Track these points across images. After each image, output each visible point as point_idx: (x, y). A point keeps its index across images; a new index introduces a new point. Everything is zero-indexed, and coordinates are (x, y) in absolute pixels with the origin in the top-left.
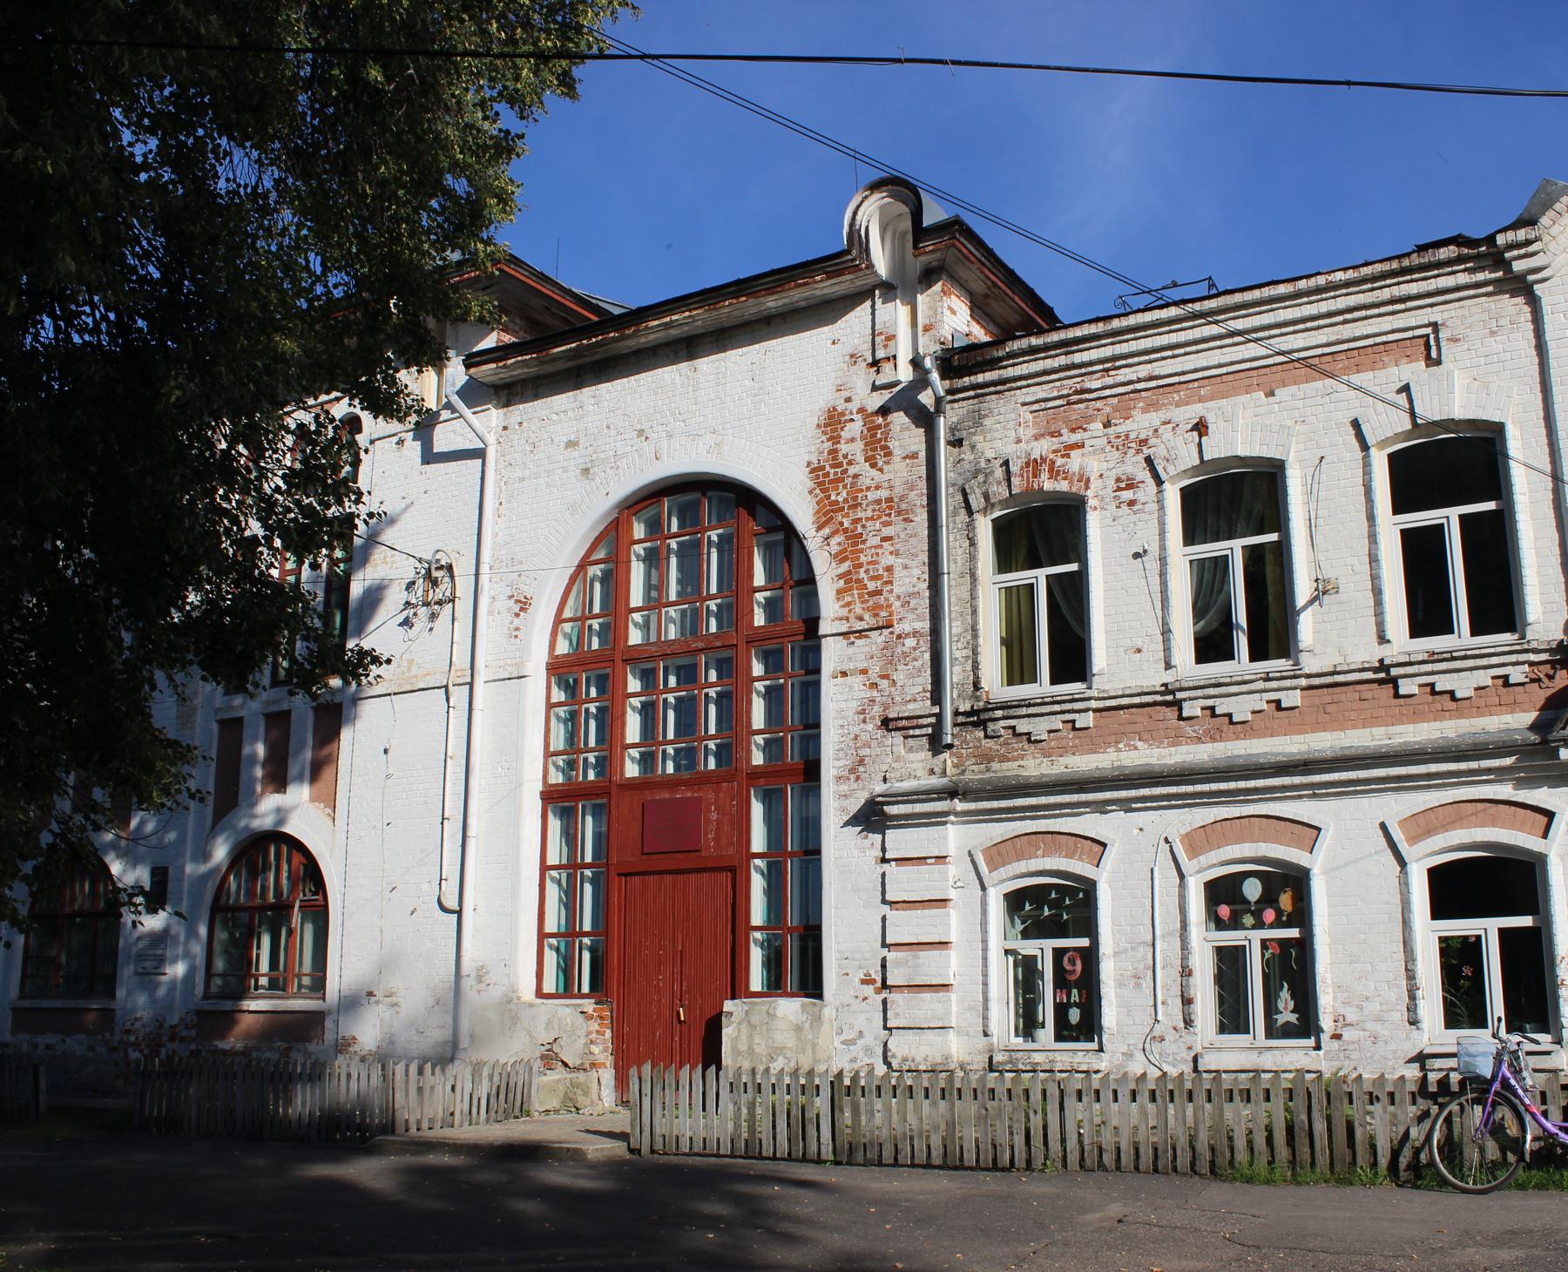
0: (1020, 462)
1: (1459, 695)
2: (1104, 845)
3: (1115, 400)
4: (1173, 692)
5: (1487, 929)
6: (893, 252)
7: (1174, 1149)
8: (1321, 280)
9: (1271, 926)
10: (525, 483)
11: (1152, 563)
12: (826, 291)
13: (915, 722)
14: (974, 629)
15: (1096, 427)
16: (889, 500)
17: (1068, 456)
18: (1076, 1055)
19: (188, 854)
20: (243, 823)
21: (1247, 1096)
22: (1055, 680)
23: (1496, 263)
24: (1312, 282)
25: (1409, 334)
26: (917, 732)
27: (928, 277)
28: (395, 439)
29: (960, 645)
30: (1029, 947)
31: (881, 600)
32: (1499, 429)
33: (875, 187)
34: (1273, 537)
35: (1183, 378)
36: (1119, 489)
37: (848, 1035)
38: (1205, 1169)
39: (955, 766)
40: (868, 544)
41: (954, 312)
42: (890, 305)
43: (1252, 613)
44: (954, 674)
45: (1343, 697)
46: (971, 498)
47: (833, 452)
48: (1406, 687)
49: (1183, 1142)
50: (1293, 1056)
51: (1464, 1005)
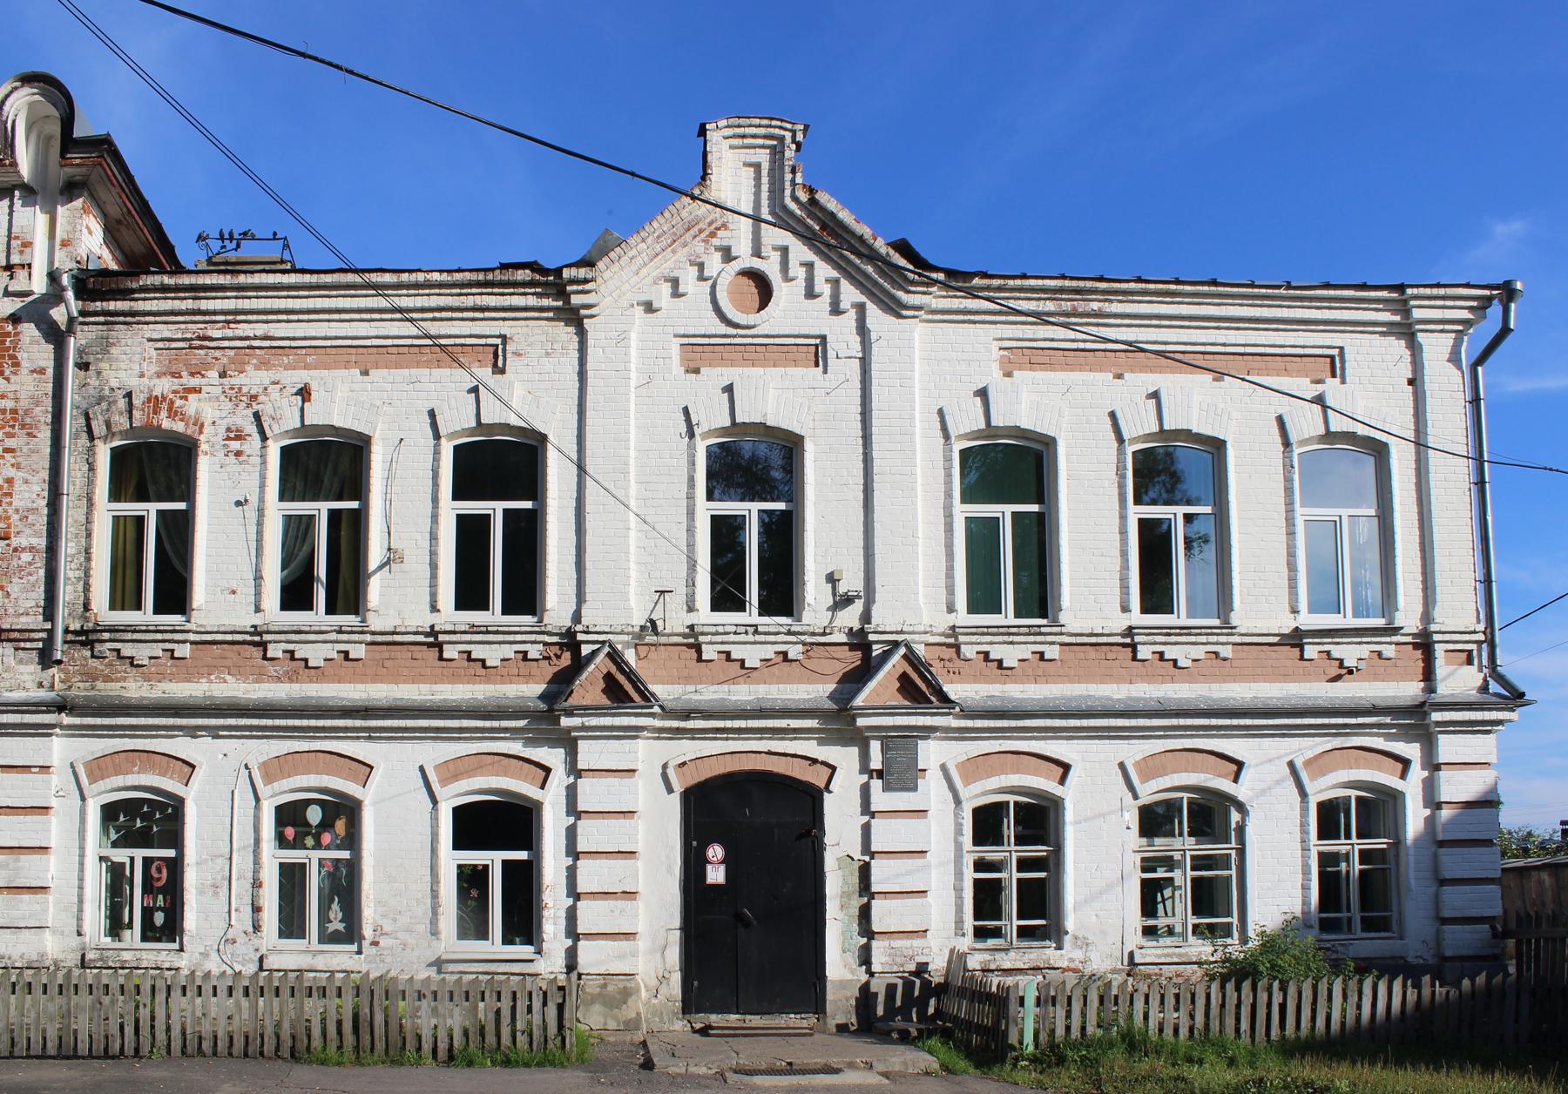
0: (143, 397)
1: (488, 663)
2: (193, 767)
3: (232, 353)
4: (260, 634)
5: (493, 859)
6: (37, 154)
7: (262, 1036)
8: (421, 277)
9: (328, 848)
13: (26, 635)
14: (88, 551)
15: (213, 375)
17: (186, 399)
18: (159, 954)
21: (323, 992)
22: (157, 611)
23: (557, 290)
24: (413, 277)
25: (482, 341)
26: (28, 645)
27: (70, 190)
29: (73, 566)
30: (121, 855)
32: (1050, 443)
33: (28, 79)
34: (354, 505)
35: (294, 344)
36: (228, 438)
38: (287, 1054)
39: (62, 681)
41: (90, 233)
42: (29, 210)
43: (327, 570)
44: (67, 593)
45: (398, 655)
46: (94, 424)
48: (449, 652)
49: (269, 1031)
50: (340, 958)
51: (473, 923)
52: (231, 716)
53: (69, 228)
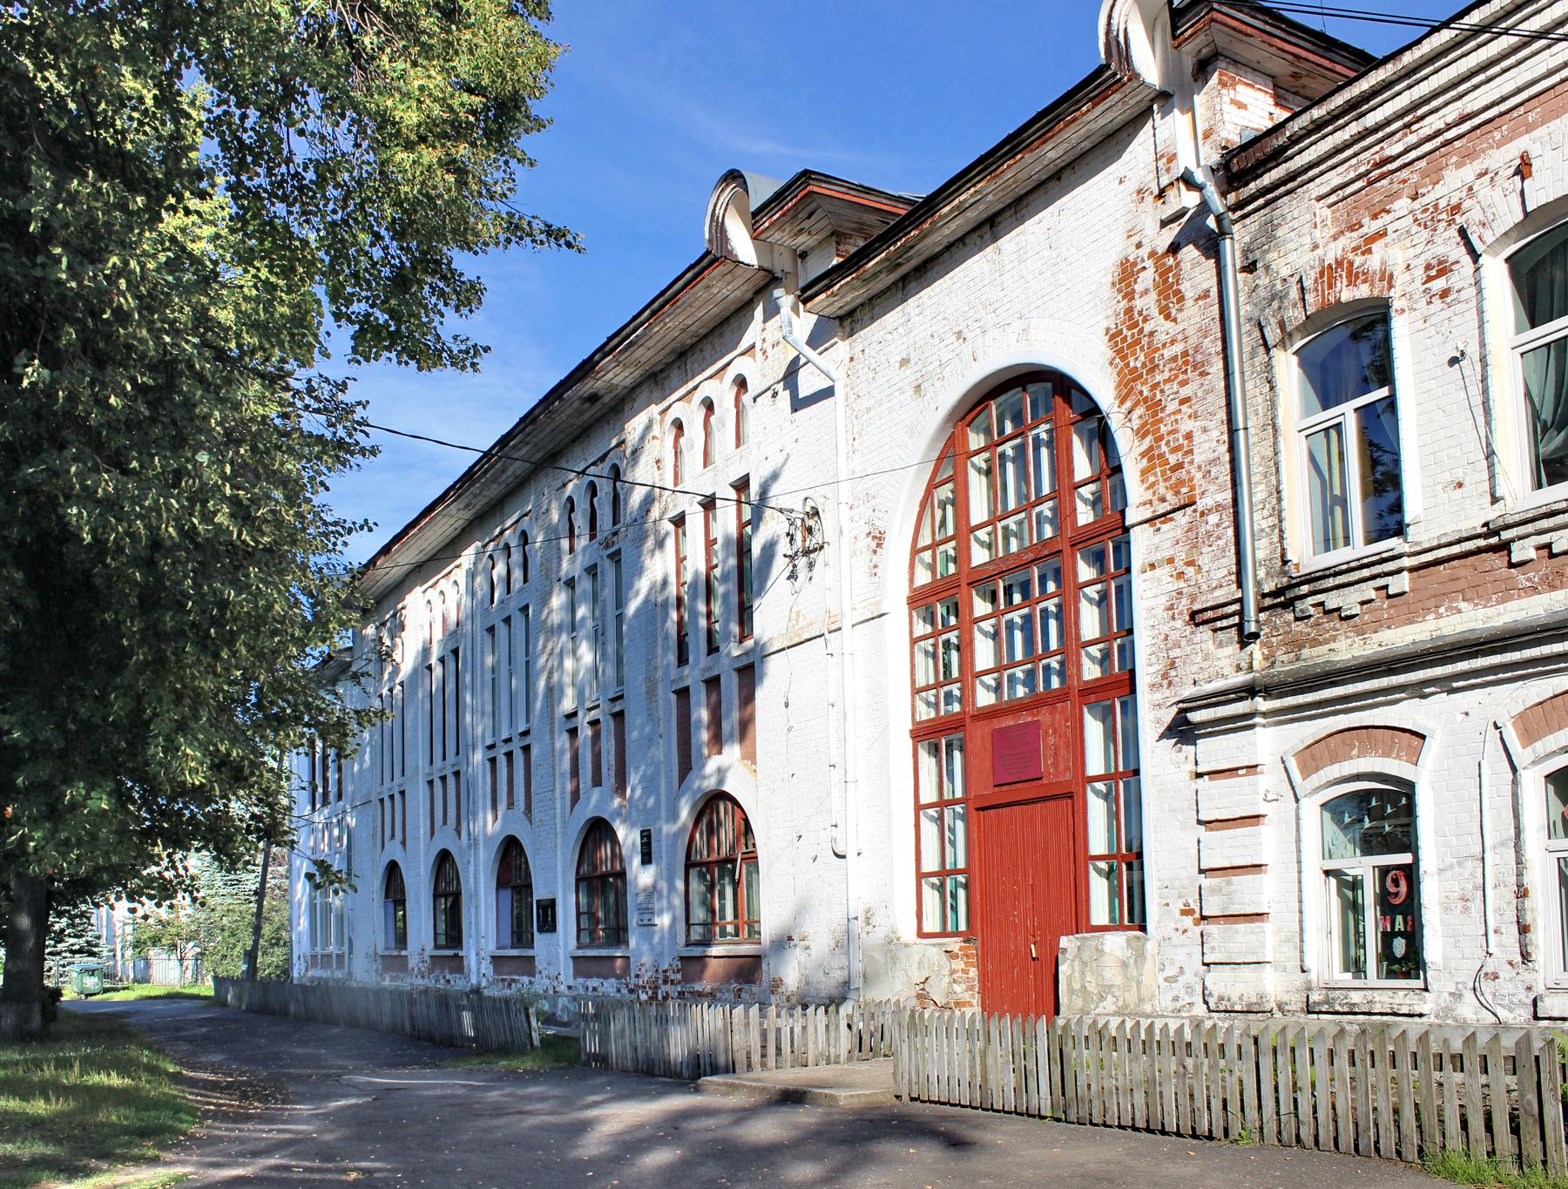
0: (1313, 274)
2: (1423, 737)
4: (1496, 533)
10: (872, 413)
11: (1470, 368)
12: (1101, 122)
13: (1220, 612)
16: (1185, 354)
17: (1369, 251)
19: (663, 815)
20: (696, 785)
21: (1458, 1062)
26: (1225, 623)
27: (1203, 69)
28: (770, 393)
31: (1183, 474)
36: (1430, 279)
37: (1171, 971)
38: (1411, 1153)
40: (1168, 411)
41: (1241, 106)
44: (1260, 550)
47: (1129, 311)
52: (1462, 658)
53: (1210, 114)
